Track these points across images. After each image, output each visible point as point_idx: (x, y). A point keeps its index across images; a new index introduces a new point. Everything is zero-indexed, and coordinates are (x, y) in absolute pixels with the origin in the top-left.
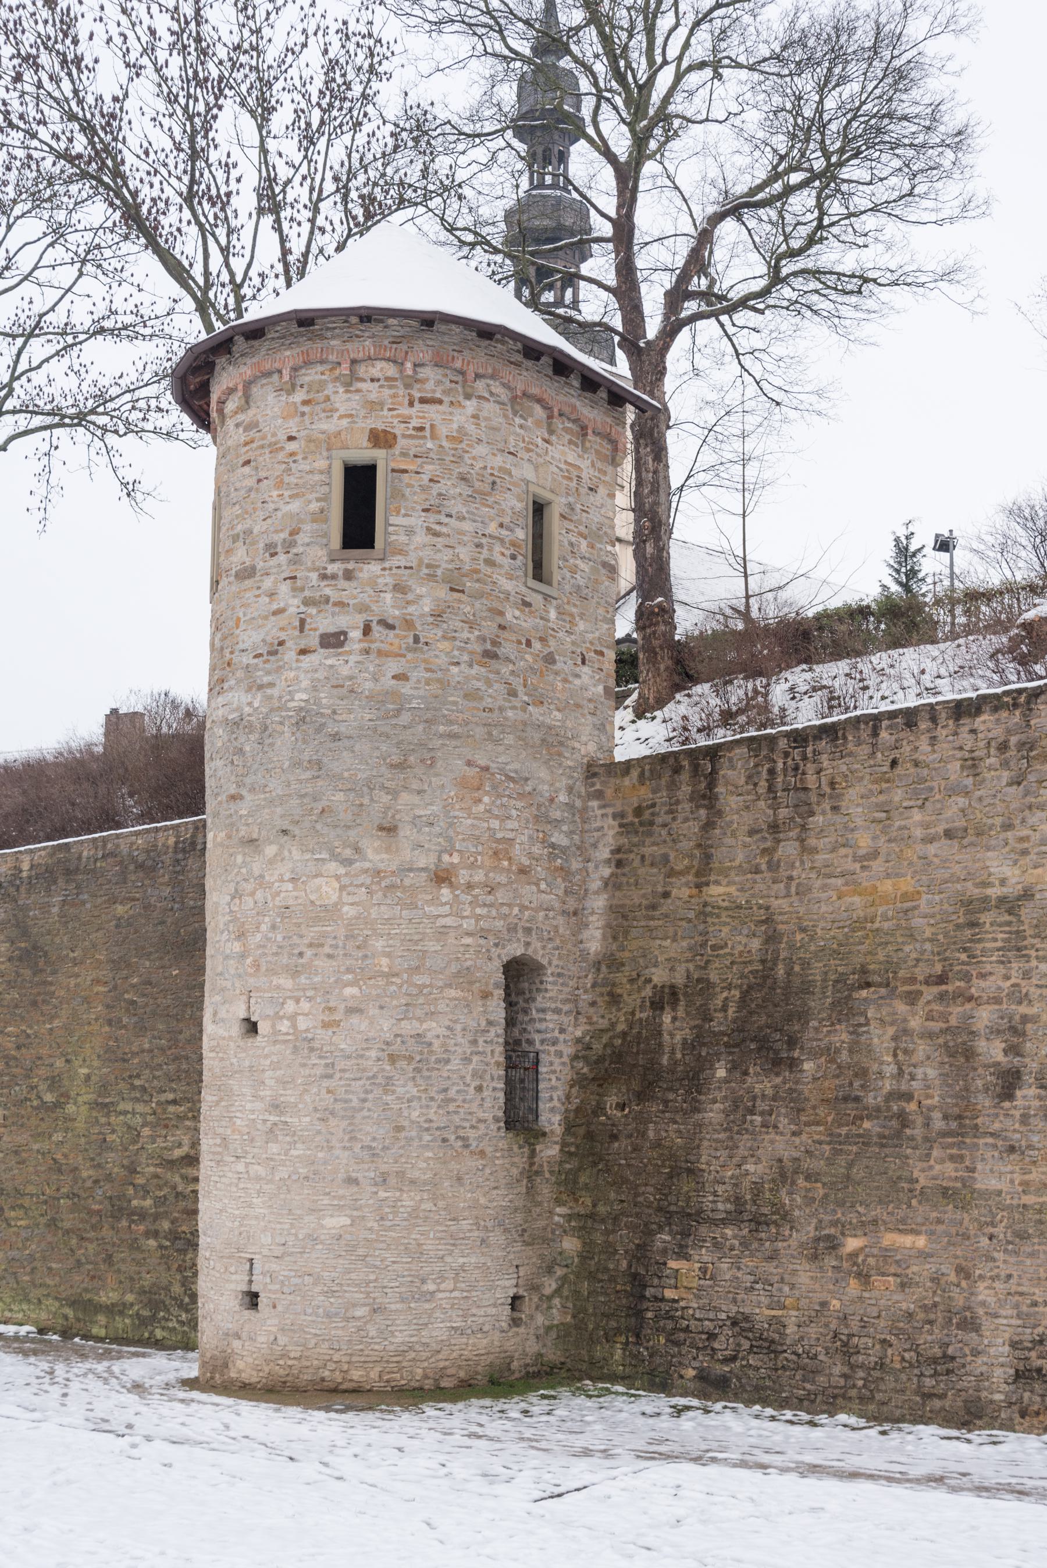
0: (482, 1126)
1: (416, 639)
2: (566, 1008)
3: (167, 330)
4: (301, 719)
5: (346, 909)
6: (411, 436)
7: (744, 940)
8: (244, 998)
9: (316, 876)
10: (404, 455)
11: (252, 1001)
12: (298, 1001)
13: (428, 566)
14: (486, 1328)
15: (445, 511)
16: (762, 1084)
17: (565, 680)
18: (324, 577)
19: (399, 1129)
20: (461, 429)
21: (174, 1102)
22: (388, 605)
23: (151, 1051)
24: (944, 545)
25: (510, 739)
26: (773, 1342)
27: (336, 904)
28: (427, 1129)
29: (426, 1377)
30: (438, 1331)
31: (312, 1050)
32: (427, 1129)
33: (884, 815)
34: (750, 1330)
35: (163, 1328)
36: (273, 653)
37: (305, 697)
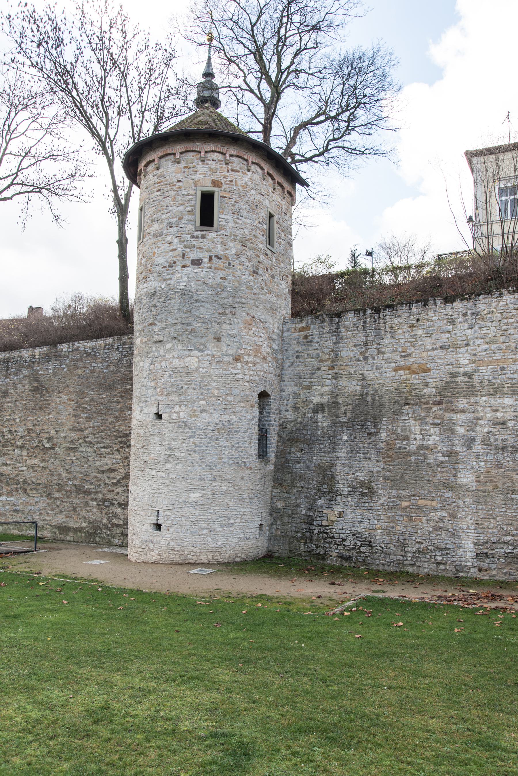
0: (251, 457)
1: (229, 264)
2: (276, 412)
3: (76, 157)
4: (183, 294)
5: (201, 369)
6: (227, 184)
7: (353, 387)
8: (156, 405)
9: (188, 356)
10: (225, 191)
11: (160, 406)
12: (180, 406)
13: (234, 235)
14: (251, 537)
15: (240, 214)
16: (363, 443)
17: (277, 286)
18: (193, 237)
19: (221, 458)
20: (246, 183)
21: (104, 447)
22: (219, 250)
23: (93, 427)
24: (370, 254)
25: (261, 306)
26: (371, 542)
27: (197, 367)
28: (232, 458)
29: (230, 557)
30: (234, 540)
31: (186, 426)
32: (232, 458)
33: (414, 340)
34: (360, 537)
35: (99, 537)
36: (171, 266)
37: (185, 284)
